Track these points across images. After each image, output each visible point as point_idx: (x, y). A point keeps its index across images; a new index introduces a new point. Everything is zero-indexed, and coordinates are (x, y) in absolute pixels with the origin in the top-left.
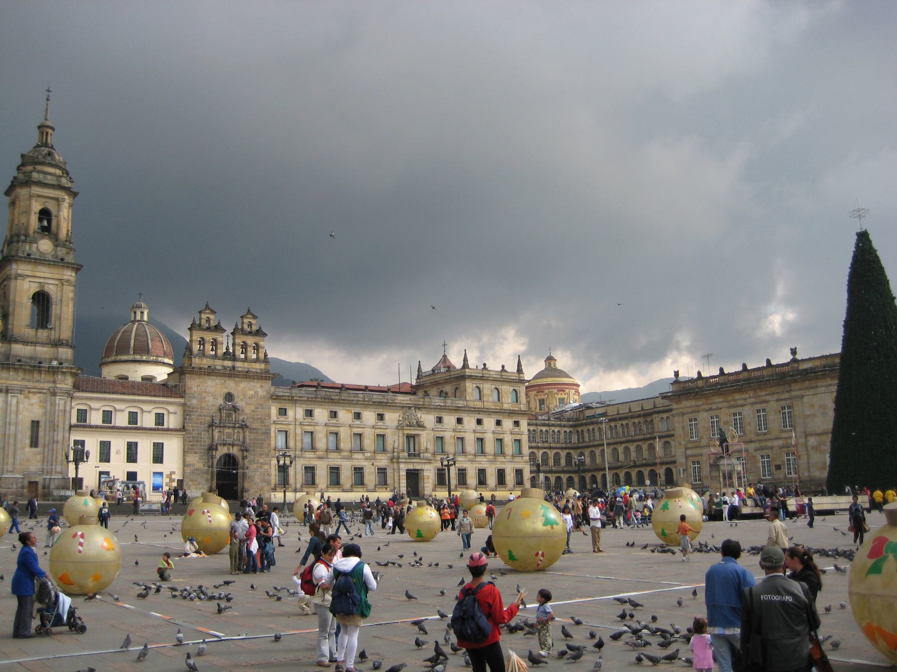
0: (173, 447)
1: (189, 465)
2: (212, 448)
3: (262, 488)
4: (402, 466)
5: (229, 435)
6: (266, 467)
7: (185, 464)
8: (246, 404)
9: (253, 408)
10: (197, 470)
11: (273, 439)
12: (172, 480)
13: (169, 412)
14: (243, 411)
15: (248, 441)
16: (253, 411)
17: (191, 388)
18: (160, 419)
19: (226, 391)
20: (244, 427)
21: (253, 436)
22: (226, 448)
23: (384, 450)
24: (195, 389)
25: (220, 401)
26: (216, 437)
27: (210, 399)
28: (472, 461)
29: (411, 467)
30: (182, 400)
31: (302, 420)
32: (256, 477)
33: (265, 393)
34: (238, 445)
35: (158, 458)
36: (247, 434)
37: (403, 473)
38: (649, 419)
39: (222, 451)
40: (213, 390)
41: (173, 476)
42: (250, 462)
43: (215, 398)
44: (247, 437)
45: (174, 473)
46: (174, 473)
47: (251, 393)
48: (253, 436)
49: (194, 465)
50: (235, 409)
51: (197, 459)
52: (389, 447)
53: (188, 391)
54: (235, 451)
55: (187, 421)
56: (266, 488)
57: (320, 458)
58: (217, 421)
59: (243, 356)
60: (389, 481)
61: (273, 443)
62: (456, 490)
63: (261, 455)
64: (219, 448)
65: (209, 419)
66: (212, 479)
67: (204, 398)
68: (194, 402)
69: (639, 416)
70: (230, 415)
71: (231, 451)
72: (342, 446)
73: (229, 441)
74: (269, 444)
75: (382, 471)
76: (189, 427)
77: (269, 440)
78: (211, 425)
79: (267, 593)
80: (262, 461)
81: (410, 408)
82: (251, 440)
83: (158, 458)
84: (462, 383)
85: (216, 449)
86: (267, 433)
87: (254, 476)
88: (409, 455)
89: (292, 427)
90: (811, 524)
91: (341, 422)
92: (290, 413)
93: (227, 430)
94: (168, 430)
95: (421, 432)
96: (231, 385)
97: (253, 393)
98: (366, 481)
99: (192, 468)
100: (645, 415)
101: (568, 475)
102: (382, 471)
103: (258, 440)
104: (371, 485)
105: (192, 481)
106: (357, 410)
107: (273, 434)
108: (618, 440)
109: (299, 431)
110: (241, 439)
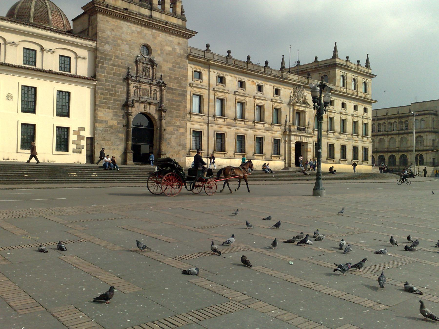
0: (81, 98)
1: (101, 122)
2: (127, 105)
3: (178, 152)
4: (293, 138)
5: (146, 93)
6: (182, 130)
7: (95, 120)
8: (164, 60)
9: (170, 66)
10: (111, 127)
11: (189, 102)
12: (81, 138)
13: (77, 57)
14: (161, 67)
15: (165, 102)
16: (170, 69)
17: (103, 31)
18: (65, 62)
19: (142, 42)
20: (161, 85)
21: (170, 97)
22: (142, 106)
23: (278, 122)
24: (109, 33)
25: (137, 52)
26: (132, 93)
27: (125, 47)
28: (338, 138)
29: (299, 140)
30: (94, 44)
31: (215, 86)
32: (173, 140)
33: (182, 52)
34: (154, 104)
35: (64, 110)
36: (164, 93)
37: (293, 145)
38: (404, 120)
39: (137, 109)
40: (129, 38)
41: (82, 133)
42: (169, 123)
43: (131, 47)
44: (165, 97)
45: (83, 129)
46: (83, 129)
47: (169, 49)
48: (170, 97)
49: (106, 122)
50: (152, 63)
51: (111, 114)
52: (283, 121)
53: (99, 34)
54: (152, 110)
55: (99, 69)
56: (182, 152)
57: (229, 125)
58: (133, 73)
59: (159, 7)
60: (282, 152)
61: (189, 106)
62: (326, 162)
63: (177, 117)
64: (136, 104)
65: (124, 71)
66: (127, 140)
67: (119, 45)
68: (107, 48)
69: (395, 118)
70: (145, 70)
71: (148, 111)
72: (247, 115)
73: (146, 98)
74: (186, 107)
75: (277, 142)
76: (101, 75)
77: (186, 102)
78: (127, 79)
79: (422, 306)
80: (178, 123)
81: (300, 86)
82: (168, 100)
83: (64, 110)
84: (331, 72)
85: (133, 106)
86: (184, 95)
87: (170, 139)
88: (298, 129)
89: (206, 92)
90: (316, 191)
91: (247, 92)
92: (205, 77)
93: (144, 86)
94: (76, 77)
95: (307, 110)
96: (149, 35)
97: (170, 49)
98: (265, 151)
99: (104, 125)
100: (400, 117)
101: (390, 154)
102: (277, 142)
103: (175, 101)
104: (268, 156)
105: (104, 140)
106: (260, 82)
107: (189, 97)
108: (384, 133)
109: (212, 97)
110: (159, 99)
